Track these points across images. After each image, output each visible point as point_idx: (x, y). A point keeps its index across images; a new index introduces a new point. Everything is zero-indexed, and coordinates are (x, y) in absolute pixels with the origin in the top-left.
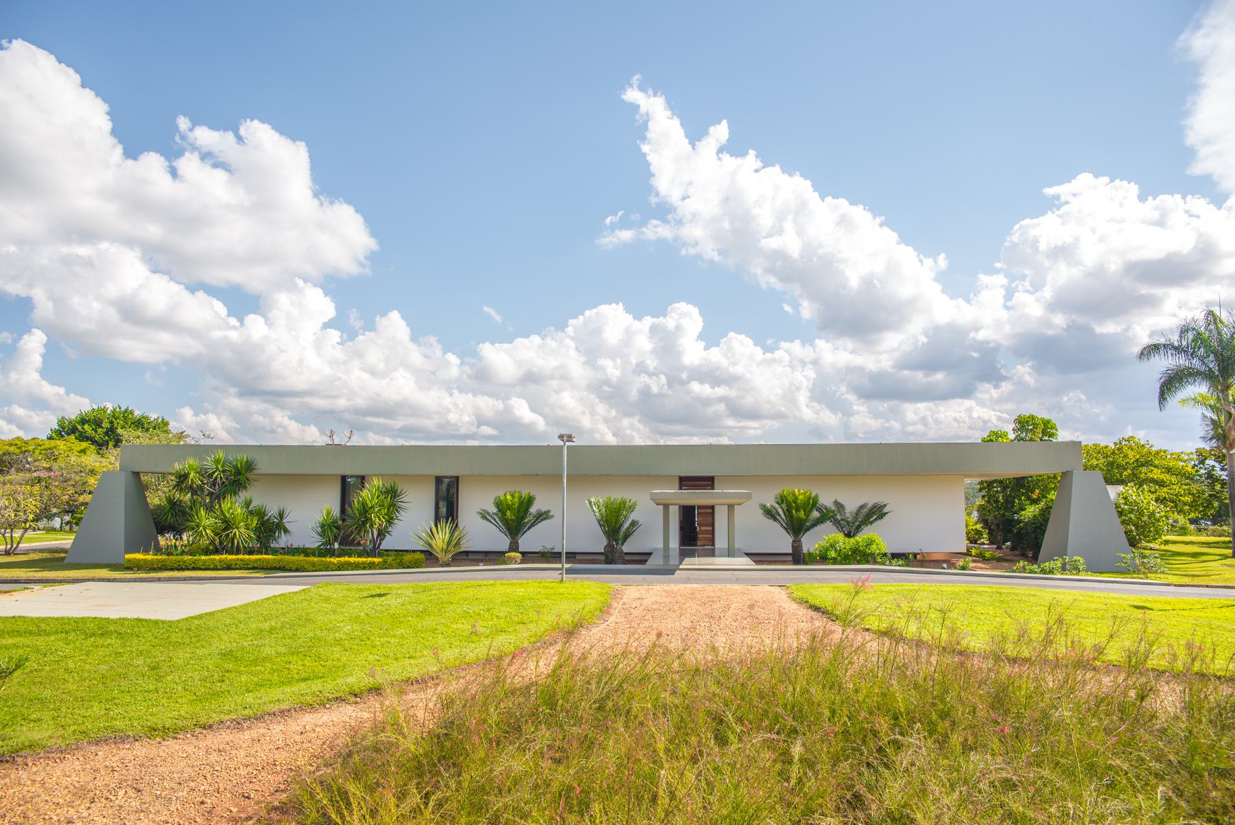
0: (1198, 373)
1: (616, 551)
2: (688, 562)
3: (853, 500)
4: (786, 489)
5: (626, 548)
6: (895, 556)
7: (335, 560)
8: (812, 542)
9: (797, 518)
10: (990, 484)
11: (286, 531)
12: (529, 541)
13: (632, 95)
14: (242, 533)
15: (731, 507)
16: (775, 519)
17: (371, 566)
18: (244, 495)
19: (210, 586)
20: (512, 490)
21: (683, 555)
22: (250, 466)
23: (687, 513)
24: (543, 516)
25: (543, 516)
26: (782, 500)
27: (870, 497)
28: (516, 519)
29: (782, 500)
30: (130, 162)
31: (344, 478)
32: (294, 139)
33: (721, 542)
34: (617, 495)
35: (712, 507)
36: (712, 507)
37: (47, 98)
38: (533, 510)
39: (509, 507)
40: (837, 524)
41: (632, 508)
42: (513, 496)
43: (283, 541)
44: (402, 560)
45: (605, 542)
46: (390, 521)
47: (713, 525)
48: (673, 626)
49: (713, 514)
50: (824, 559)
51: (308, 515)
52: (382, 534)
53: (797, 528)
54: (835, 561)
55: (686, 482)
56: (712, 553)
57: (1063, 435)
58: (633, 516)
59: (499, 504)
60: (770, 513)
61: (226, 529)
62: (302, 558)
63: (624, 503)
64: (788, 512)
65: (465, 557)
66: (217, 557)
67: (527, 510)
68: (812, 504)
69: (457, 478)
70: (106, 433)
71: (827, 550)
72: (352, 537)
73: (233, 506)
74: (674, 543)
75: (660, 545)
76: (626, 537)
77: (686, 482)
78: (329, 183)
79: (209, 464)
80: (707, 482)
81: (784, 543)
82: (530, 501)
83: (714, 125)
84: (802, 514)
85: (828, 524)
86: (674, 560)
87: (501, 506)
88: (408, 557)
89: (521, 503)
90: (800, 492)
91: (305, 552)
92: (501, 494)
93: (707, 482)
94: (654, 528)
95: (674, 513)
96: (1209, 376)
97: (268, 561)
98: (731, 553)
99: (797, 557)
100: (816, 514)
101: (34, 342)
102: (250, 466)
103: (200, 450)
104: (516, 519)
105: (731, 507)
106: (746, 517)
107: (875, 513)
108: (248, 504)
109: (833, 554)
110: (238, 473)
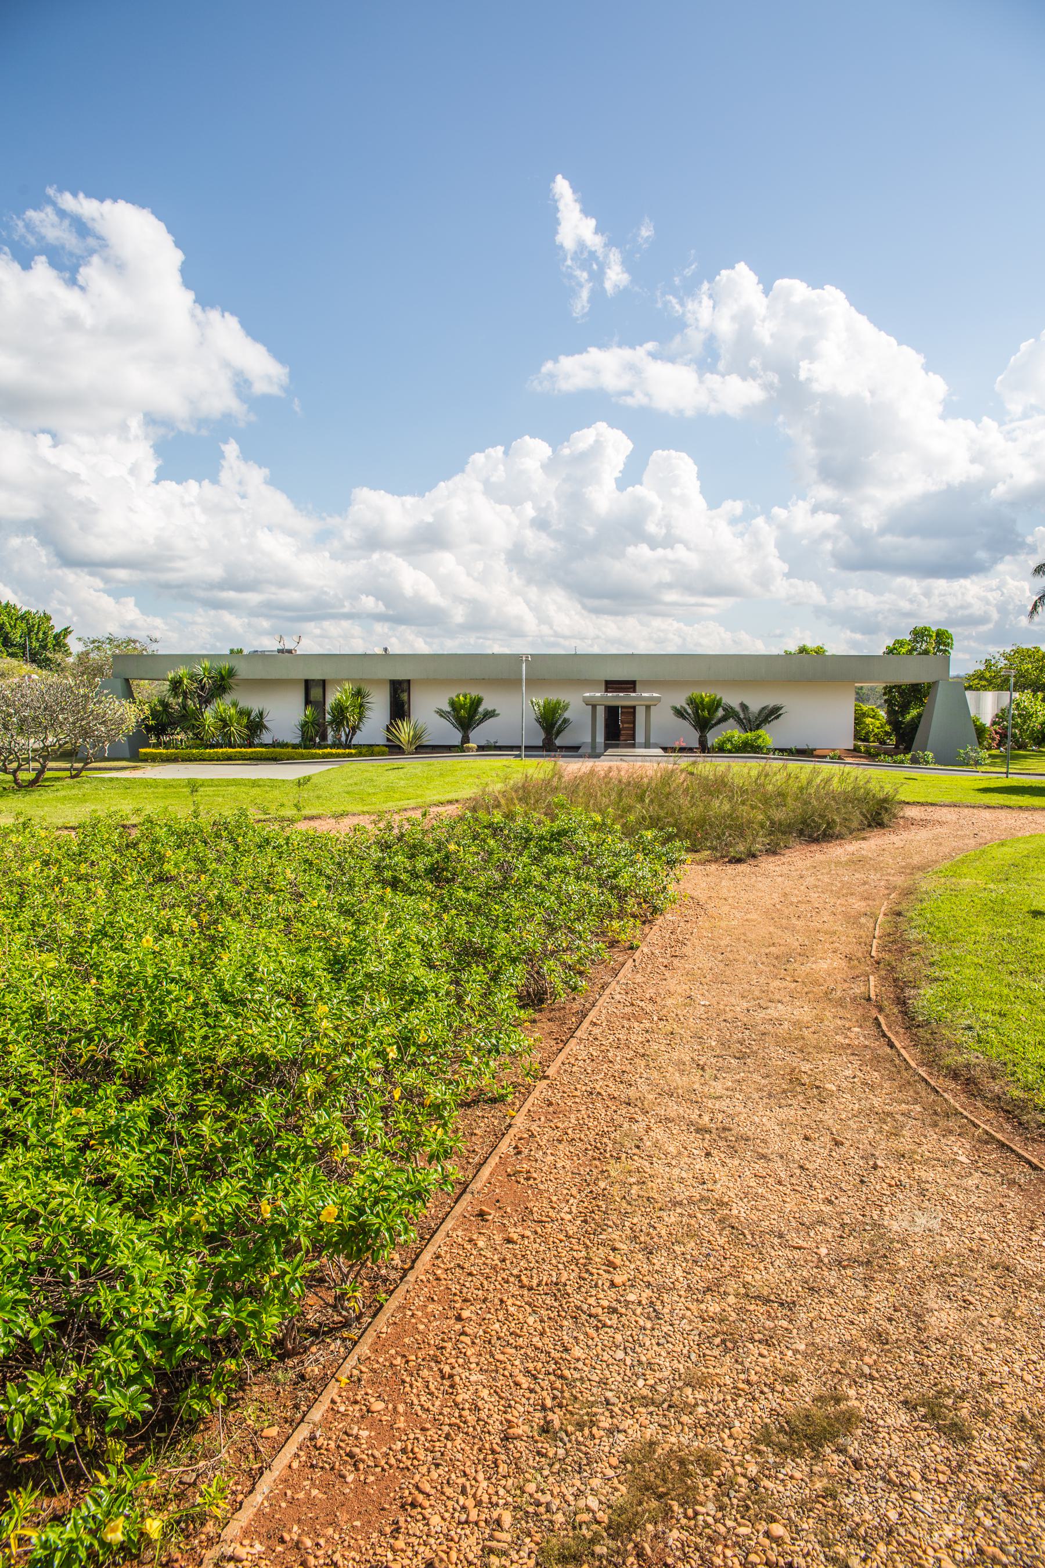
2: (610, 751)
5: (558, 742)
6: (782, 750)
7: (320, 751)
8: (714, 738)
9: (703, 717)
10: (891, 688)
11: (266, 728)
12: (479, 735)
13: (562, 186)
16: (684, 718)
17: (350, 755)
18: (228, 698)
19: (492, 759)
20: (463, 692)
21: (607, 747)
22: (231, 673)
23: (612, 712)
24: (489, 714)
25: (489, 714)
26: (691, 702)
27: (771, 701)
29: (691, 702)
31: (307, 683)
33: (640, 738)
34: (555, 696)
35: (634, 708)
36: (634, 708)
38: (481, 709)
39: (462, 707)
40: (740, 721)
41: (565, 708)
42: (465, 697)
43: (266, 738)
44: (369, 751)
45: (543, 736)
46: (360, 719)
47: (634, 723)
48: (873, 786)
49: (634, 713)
50: (721, 749)
51: (285, 715)
52: (354, 729)
53: (703, 725)
54: (730, 751)
55: (611, 685)
56: (633, 746)
57: (245, 652)
58: (566, 715)
59: (452, 704)
60: (680, 713)
61: (224, 727)
62: (290, 750)
64: (696, 713)
65: (423, 749)
66: (220, 750)
67: (476, 710)
69: (324, 681)
71: (724, 742)
72: (325, 732)
73: (222, 706)
74: (600, 739)
79: (199, 670)
81: (692, 737)
82: (478, 702)
83: (555, 232)
84: (706, 713)
85: (731, 721)
88: (376, 749)
89: (472, 703)
90: (706, 694)
92: (454, 696)
93: (629, 685)
95: (601, 712)
97: (261, 753)
98: (647, 745)
99: (704, 748)
102: (231, 673)
103: (188, 659)
105: (648, 707)
107: (771, 714)
109: (729, 746)
110: (223, 678)
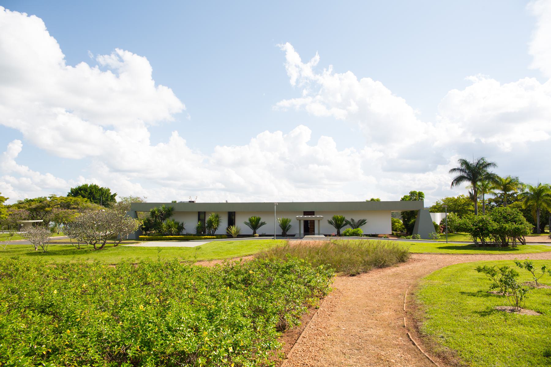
0: (467, 178)
1: (285, 232)
2: (306, 236)
3: (357, 219)
4: (335, 215)
8: (342, 231)
9: (338, 224)
12: (259, 231)
14: (174, 230)
15: (319, 221)
17: (214, 238)
18: (171, 218)
21: (305, 235)
23: (306, 222)
24: (263, 224)
25: (263, 224)
26: (334, 218)
28: (255, 225)
30: (69, 67)
32: (142, 56)
33: (316, 231)
34: (286, 217)
37: (28, 36)
38: (260, 222)
39: (253, 221)
40: (351, 225)
41: (290, 221)
43: (184, 232)
44: (220, 237)
50: (345, 235)
52: (215, 229)
55: (306, 213)
56: (314, 234)
58: (290, 224)
59: (250, 220)
60: (330, 223)
63: (287, 219)
68: (343, 219)
70: (89, 194)
74: (302, 232)
75: (298, 232)
76: (288, 230)
77: (306, 213)
78: (159, 78)
80: (312, 213)
82: (259, 219)
86: (302, 236)
87: (250, 220)
90: (339, 216)
91: (191, 235)
92: (251, 217)
93: (312, 213)
94: (296, 227)
96: (469, 179)
98: (319, 234)
99: (339, 234)
100: (344, 222)
101: (16, 147)
104: (255, 225)
106: (323, 222)
107: (362, 223)
108: (173, 220)
110: (169, 211)
